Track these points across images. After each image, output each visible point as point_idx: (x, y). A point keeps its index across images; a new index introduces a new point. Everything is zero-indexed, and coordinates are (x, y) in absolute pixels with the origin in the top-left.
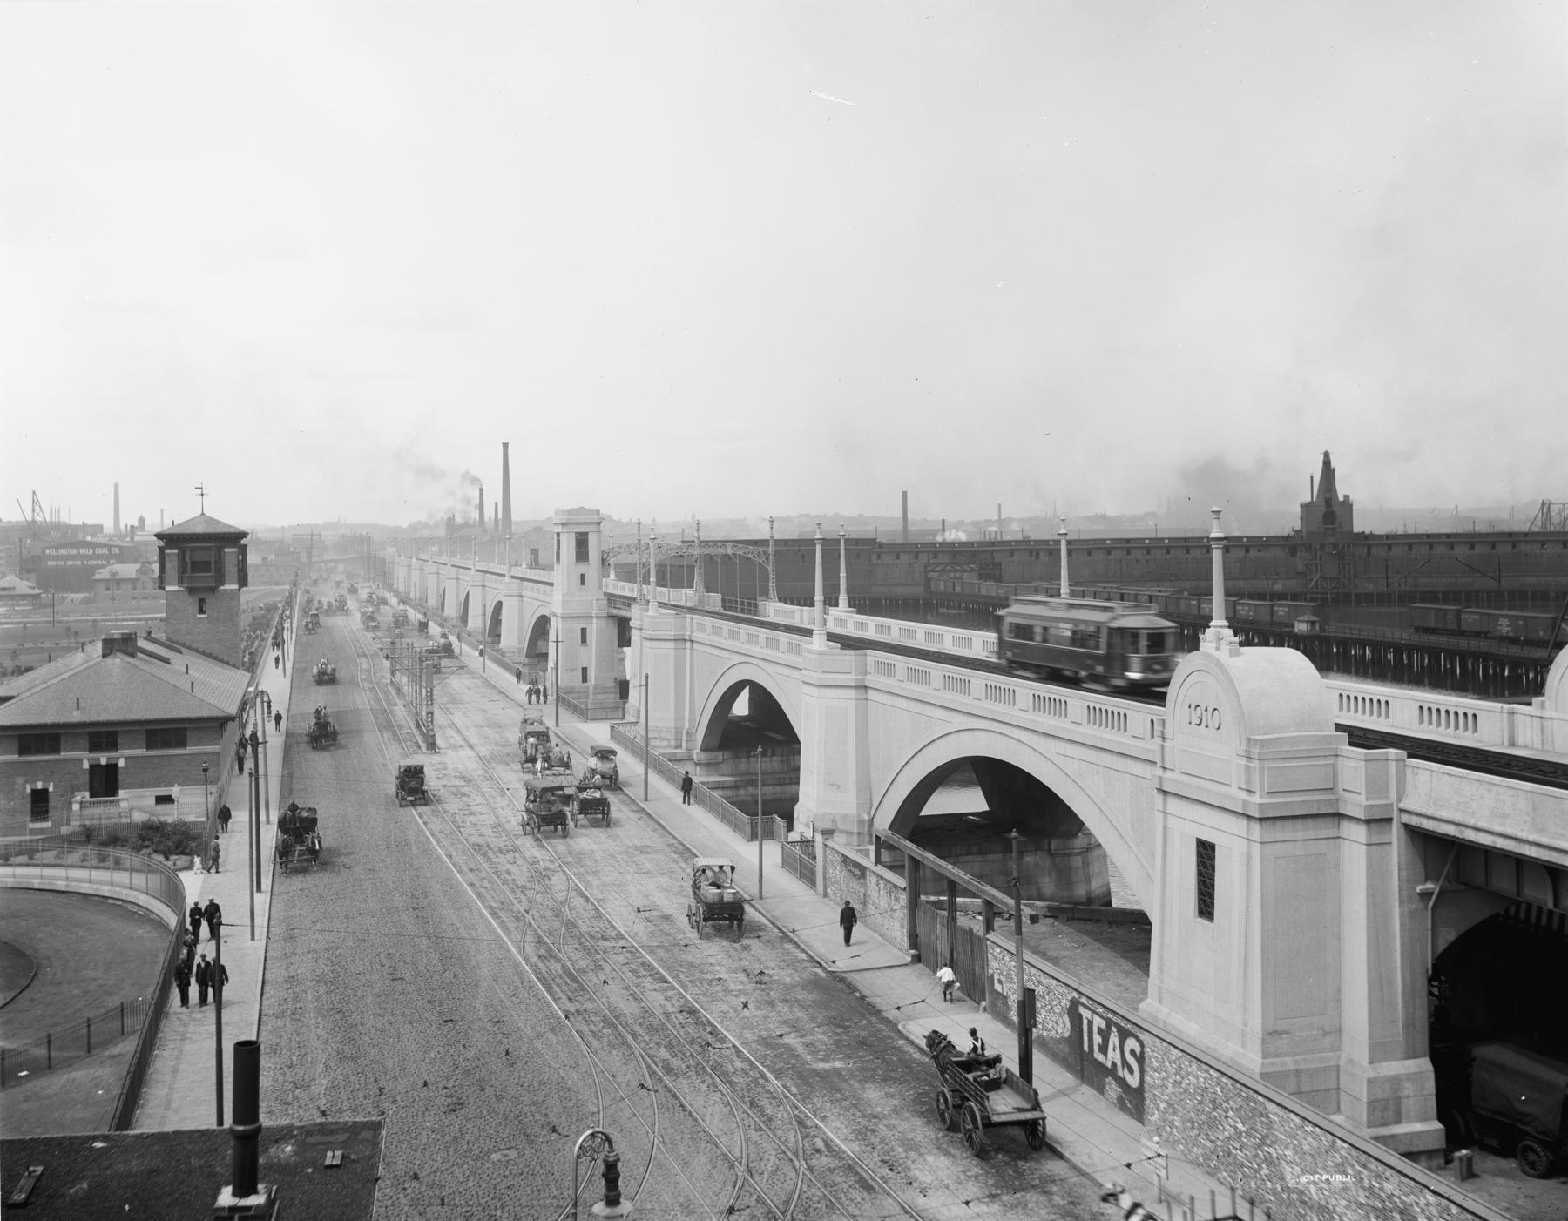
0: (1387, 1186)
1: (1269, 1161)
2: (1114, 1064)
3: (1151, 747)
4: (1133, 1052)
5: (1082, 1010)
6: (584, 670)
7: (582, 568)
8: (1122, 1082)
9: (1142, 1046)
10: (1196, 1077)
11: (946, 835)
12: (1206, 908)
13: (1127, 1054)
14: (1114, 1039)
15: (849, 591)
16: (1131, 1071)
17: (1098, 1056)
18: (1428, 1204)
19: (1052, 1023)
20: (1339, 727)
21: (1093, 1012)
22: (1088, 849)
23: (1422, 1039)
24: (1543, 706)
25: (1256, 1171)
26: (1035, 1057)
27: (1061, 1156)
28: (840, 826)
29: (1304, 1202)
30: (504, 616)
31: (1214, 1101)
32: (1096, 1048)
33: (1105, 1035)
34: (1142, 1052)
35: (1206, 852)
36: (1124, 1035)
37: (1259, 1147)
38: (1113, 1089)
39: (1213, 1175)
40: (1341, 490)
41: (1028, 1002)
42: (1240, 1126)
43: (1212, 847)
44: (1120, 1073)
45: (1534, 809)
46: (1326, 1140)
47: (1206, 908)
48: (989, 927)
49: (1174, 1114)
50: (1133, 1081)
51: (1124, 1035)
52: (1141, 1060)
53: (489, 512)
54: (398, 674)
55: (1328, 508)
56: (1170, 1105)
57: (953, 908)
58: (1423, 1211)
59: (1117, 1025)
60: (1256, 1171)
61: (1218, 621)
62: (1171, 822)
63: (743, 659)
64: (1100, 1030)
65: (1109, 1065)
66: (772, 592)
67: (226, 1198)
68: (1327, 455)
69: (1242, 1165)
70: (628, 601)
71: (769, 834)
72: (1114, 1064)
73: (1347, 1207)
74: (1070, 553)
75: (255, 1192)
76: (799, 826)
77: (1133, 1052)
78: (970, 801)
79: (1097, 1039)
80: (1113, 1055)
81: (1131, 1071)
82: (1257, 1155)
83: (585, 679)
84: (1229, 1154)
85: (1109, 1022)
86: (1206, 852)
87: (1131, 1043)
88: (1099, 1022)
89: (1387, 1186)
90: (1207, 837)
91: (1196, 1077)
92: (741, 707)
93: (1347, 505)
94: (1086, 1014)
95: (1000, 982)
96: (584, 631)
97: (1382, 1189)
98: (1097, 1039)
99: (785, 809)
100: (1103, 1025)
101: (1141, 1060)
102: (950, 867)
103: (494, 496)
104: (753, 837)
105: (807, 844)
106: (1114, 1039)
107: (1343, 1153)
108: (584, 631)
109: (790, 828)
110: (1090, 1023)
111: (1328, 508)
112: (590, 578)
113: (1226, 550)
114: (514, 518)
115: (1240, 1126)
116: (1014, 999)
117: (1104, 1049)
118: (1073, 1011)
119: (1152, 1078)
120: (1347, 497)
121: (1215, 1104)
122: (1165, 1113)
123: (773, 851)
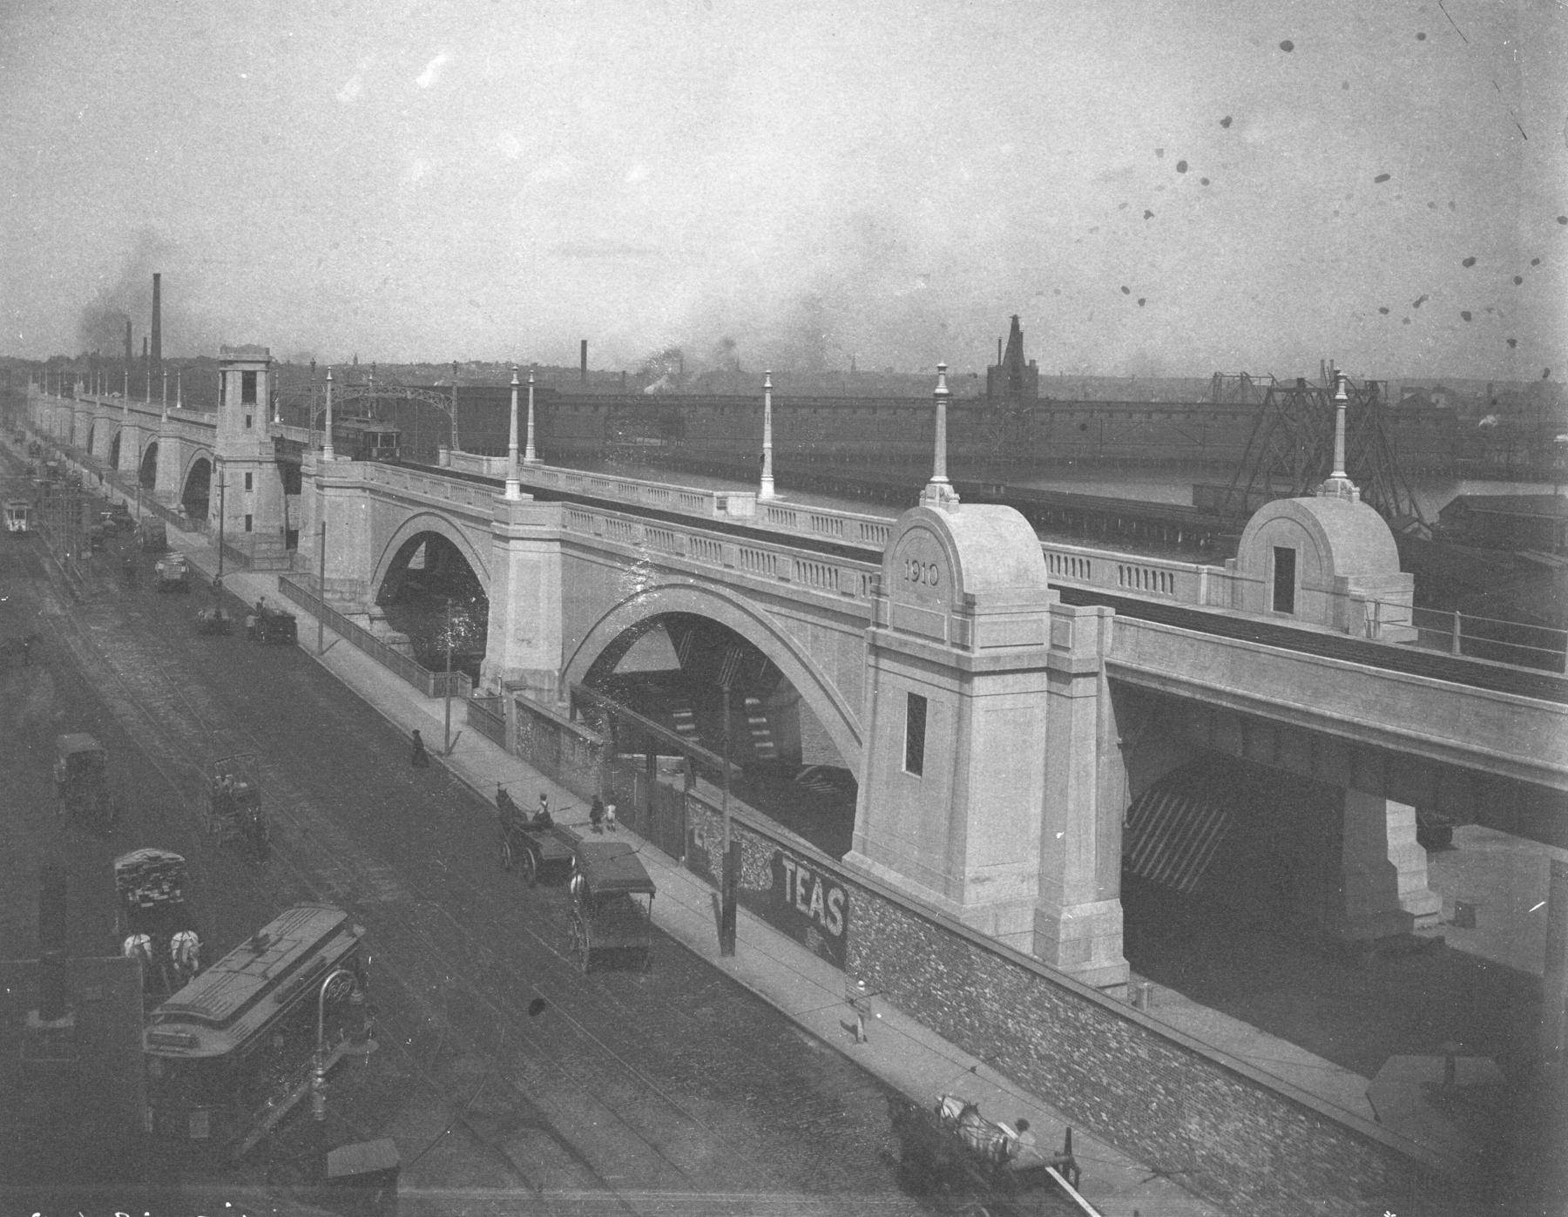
0: (1082, 1016)
1: (969, 999)
2: (816, 913)
4: (836, 901)
5: (785, 862)
6: (249, 518)
7: (248, 409)
8: (824, 931)
9: (846, 895)
10: (900, 923)
12: (915, 763)
13: (830, 903)
14: (817, 890)
17: (802, 908)
18: (1119, 1030)
19: (755, 877)
22: (796, 701)
25: (955, 1010)
26: (739, 918)
28: (530, 682)
29: (1001, 1036)
30: (160, 458)
31: (917, 946)
33: (808, 885)
34: (846, 901)
35: (917, 706)
36: (828, 886)
37: (960, 987)
38: (814, 938)
40: (1030, 353)
41: (732, 859)
42: (941, 968)
44: (823, 922)
45: (1233, 662)
46: (1026, 978)
47: (915, 763)
48: (690, 783)
49: (878, 959)
50: (836, 930)
51: (828, 886)
52: (844, 909)
53: (137, 350)
55: (1013, 369)
56: (873, 952)
57: (651, 765)
58: (1115, 1036)
59: (820, 876)
60: (955, 1010)
61: (940, 478)
62: (882, 677)
63: (425, 509)
64: (804, 882)
65: (812, 914)
69: (942, 1005)
70: (298, 447)
72: (816, 913)
73: (1042, 1038)
76: (485, 683)
77: (836, 901)
79: (801, 890)
80: (816, 905)
81: (834, 920)
82: (956, 995)
84: (930, 995)
85: (813, 874)
86: (917, 706)
87: (836, 894)
88: (801, 873)
89: (1082, 1016)
90: (919, 690)
91: (900, 923)
92: (417, 562)
93: (1032, 369)
94: (789, 866)
95: (701, 837)
96: (249, 477)
98: (801, 890)
99: (469, 661)
100: (808, 876)
101: (844, 909)
103: (144, 330)
104: (438, 693)
105: (492, 698)
106: (817, 890)
107: (646, 553)
108: (249, 477)
109: (476, 684)
110: (794, 874)
111: (1013, 369)
113: (949, 410)
115: (941, 968)
116: (716, 856)
117: (807, 900)
118: (776, 864)
119: (856, 925)
120: (1033, 362)
121: (918, 948)
122: (868, 957)
123: (460, 711)
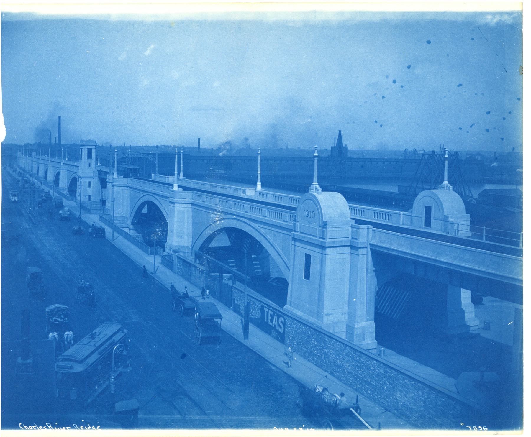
0: (362, 359)
1: (325, 353)
2: (275, 325)
3: (290, 224)
4: (281, 322)
5: (265, 309)
6: (90, 196)
7: (89, 161)
8: (277, 331)
9: (285, 319)
10: (302, 329)
11: (217, 252)
12: (307, 276)
14: (275, 318)
15: (183, 172)
16: (281, 327)
17: (270, 324)
20: (352, 219)
21: (269, 309)
23: (372, 316)
24: (412, 212)
27: (187, 396)
28: (181, 250)
30: (61, 177)
31: (308, 336)
32: (269, 321)
33: (272, 316)
34: (285, 321)
35: (308, 258)
36: (279, 316)
37: (322, 349)
38: (274, 333)
39: (306, 359)
40: (345, 142)
41: (248, 307)
42: (316, 343)
43: (310, 256)
46: (343, 347)
47: (307, 276)
48: (234, 283)
50: (281, 331)
51: (279, 316)
52: (284, 324)
53: (53, 141)
54: (95, 198)
55: (339, 148)
56: (294, 338)
58: (372, 366)
62: (297, 248)
66: (157, 171)
67: (19, 360)
68: (340, 131)
70: (106, 173)
71: (156, 253)
72: (275, 325)
74: (261, 160)
75: (29, 358)
76: (167, 250)
77: (281, 322)
78: (223, 241)
79: (270, 318)
81: (281, 327)
83: (90, 199)
85: (274, 312)
86: (308, 258)
87: (281, 319)
89: (362, 359)
90: (308, 253)
91: (302, 329)
92: (145, 210)
93: (346, 148)
94: (266, 310)
95: (237, 300)
96: (90, 183)
97: (360, 360)
98: (270, 318)
99: (162, 243)
100: (272, 313)
101: (284, 324)
102: (221, 263)
103: (55, 135)
106: (275, 318)
108: (90, 183)
109: (164, 251)
110: (268, 313)
111: (339, 148)
112: (93, 165)
114: (62, 143)
115: (316, 343)
116: (242, 307)
117: (272, 321)
118: (262, 309)
119: (288, 329)
120: (346, 145)
123: (159, 259)
